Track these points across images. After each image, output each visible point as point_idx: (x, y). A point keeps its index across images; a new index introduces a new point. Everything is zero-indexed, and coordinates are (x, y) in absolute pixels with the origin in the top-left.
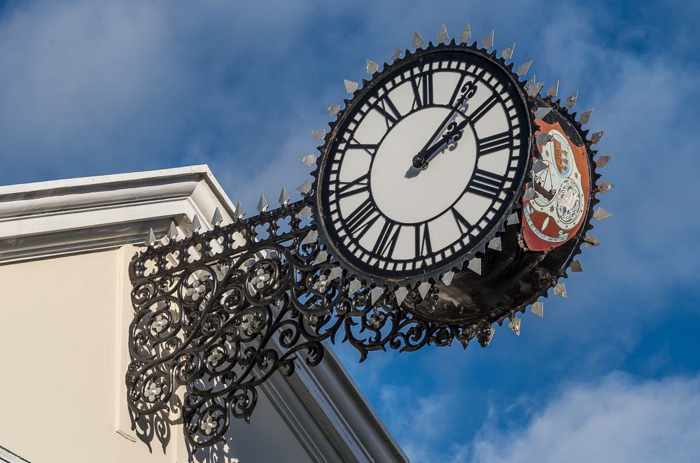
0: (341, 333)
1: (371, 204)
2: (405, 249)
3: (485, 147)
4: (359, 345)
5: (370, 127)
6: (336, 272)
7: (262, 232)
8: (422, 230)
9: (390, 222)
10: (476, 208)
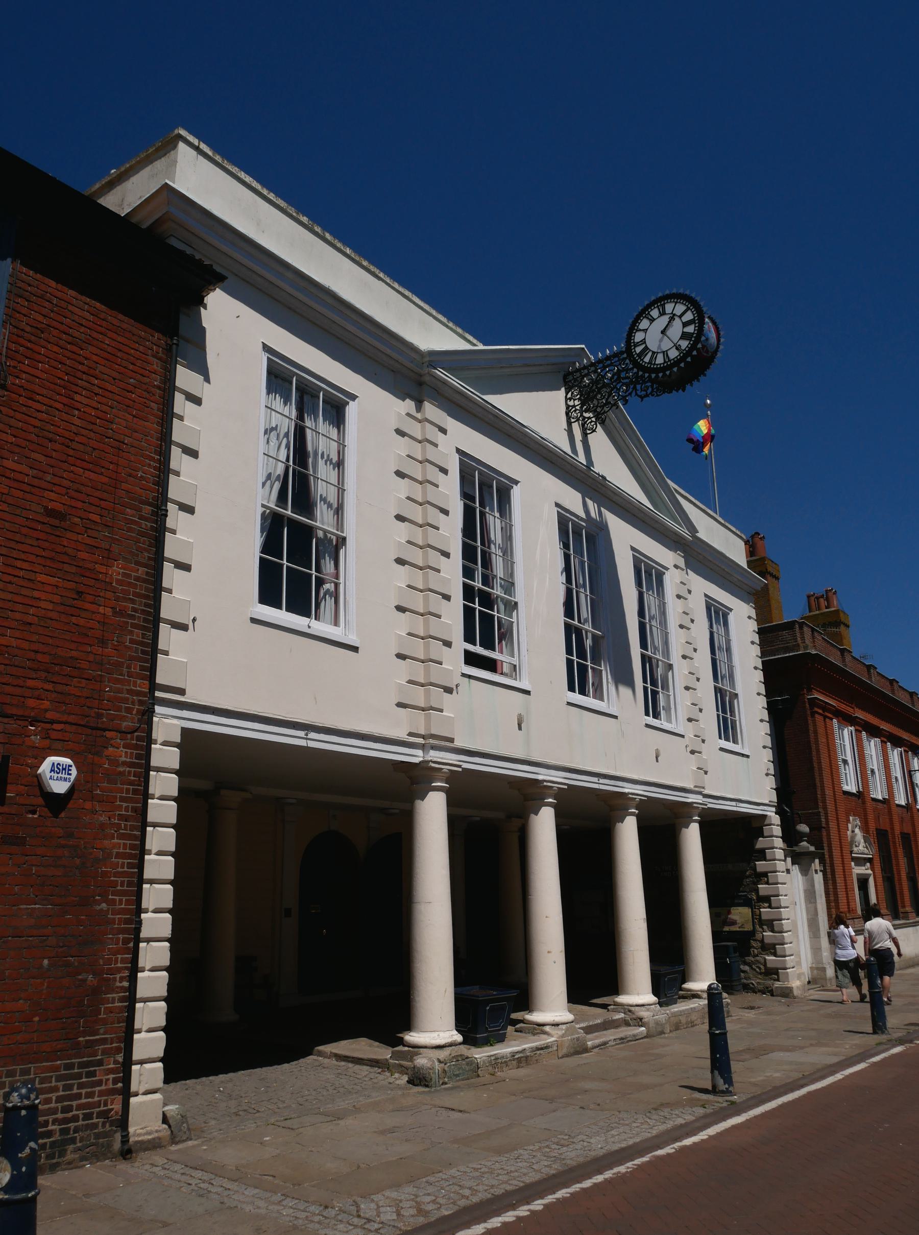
0: (634, 394)
1: (646, 348)
3: (685, 325)
5: (644, 324)
6: (635, 370)
9: (654, 353)
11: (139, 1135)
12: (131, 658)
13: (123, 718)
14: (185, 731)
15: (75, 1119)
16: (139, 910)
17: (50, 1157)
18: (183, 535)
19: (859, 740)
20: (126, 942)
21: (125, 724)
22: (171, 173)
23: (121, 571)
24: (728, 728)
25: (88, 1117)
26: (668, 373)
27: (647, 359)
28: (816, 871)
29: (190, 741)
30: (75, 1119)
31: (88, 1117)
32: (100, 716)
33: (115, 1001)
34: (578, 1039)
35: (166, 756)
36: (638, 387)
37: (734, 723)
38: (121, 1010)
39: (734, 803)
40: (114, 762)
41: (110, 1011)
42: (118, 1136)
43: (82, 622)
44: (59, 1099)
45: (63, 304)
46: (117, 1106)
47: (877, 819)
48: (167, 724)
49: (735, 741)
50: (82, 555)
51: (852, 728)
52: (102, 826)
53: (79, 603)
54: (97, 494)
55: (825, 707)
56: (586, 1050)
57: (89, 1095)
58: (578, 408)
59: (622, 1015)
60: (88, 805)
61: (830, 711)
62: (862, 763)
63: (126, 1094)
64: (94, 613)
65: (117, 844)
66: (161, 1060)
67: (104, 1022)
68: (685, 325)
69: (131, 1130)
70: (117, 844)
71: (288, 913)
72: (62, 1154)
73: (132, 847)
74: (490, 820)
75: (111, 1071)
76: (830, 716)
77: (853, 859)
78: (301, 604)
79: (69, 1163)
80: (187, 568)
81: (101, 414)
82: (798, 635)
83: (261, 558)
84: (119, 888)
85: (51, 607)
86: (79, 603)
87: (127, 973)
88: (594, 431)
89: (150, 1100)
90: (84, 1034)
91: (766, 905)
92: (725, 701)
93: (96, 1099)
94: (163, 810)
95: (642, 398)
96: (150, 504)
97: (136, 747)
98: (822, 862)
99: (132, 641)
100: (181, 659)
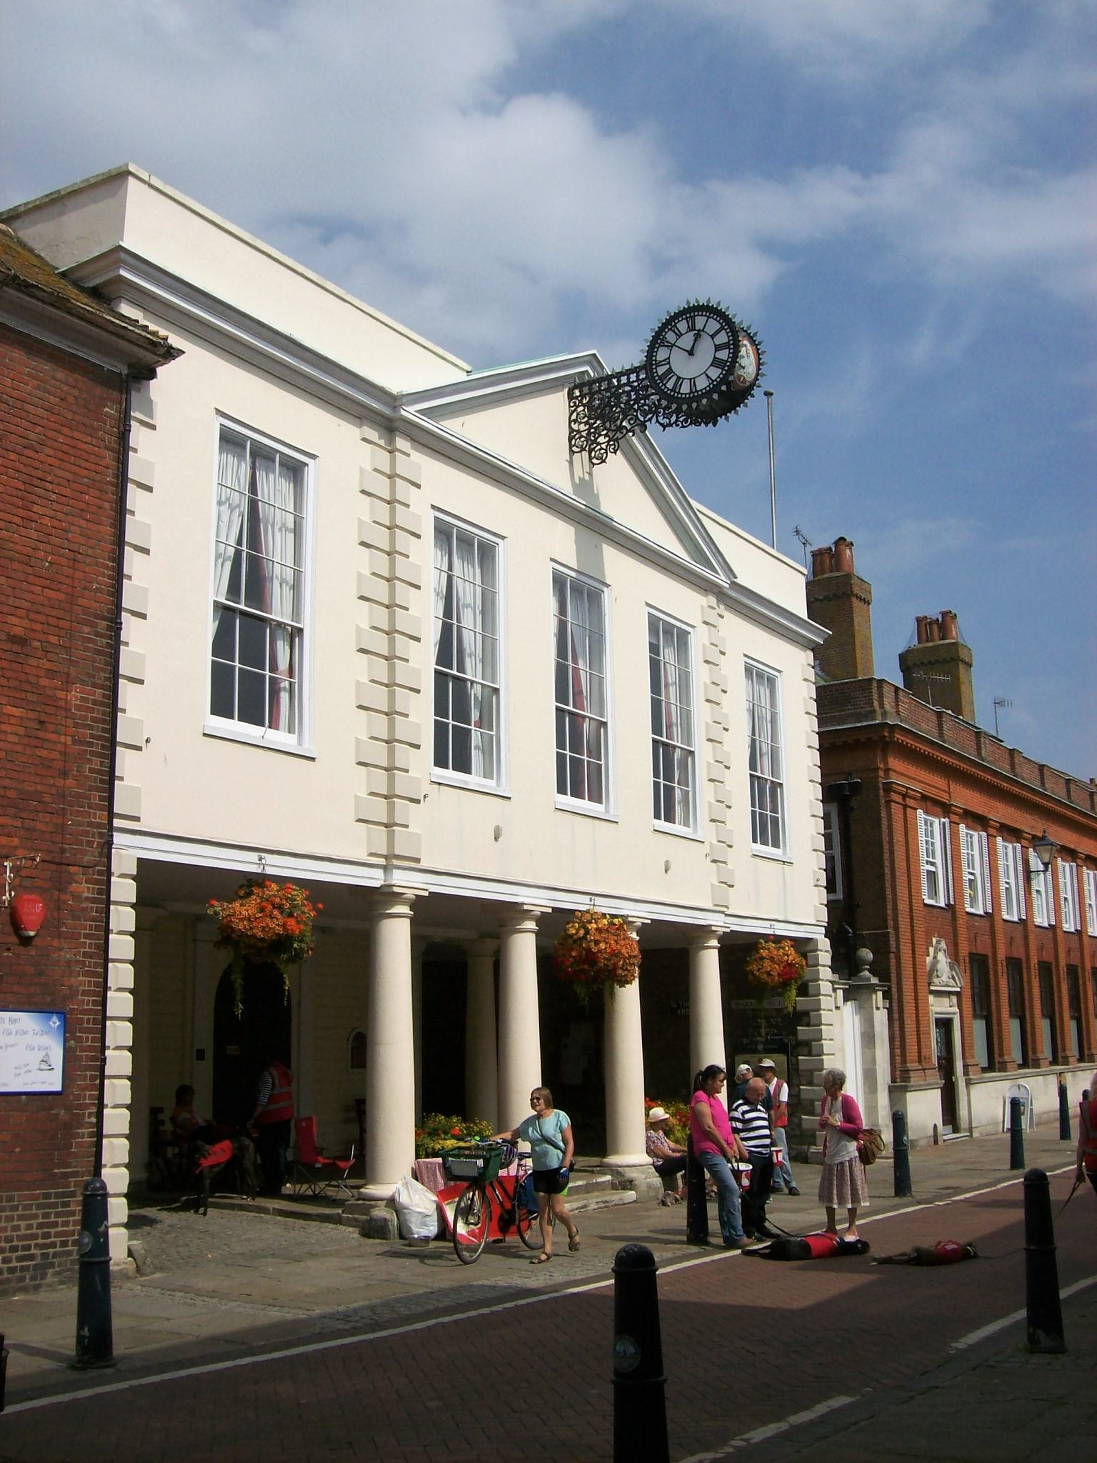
2: (685, 389)
3: (718, 348)
4: (661, 424)
7: (624, 380)
8: (692, 381)
9: (679, 378)
10: (715, 373)
12: (91, 789)
13: (85, 853)
14: (142, 862)
15: (53, 1245)
16: (103, 1048)
17: (33, 1278)
19: (955, 836)
20: (93, 1078)
21: (86, 858)
22: (121, 236)
24: (767, 828)
25: (64, 1244)
26: (694, 405)
27: (670, 385)
28: (878, 1008)
29: (148, 872)
30: (53, 1245)
31: (64, 1244)
32: (63, 851)
37: (775, 821)
38: (90, 1144)
39: (768, 924)
40: (77, 897)
41: (80, 1145)
43: (44, 753)
44: (40, 1226)
45: (19, 404)
47: (974, 939)
48: (127, 853)
49: (776, 844)
50: (44, 682)
51: (946, 820)
52: (69, 963)
53: (41, 734)
54: (55, 613)
58: (584, 434)
59: (609, 1178)
60: (56, 943)
62: (953, 862)
64: (55, 743)
66: (126, 1196)
67: (76, 1155)
68: (718, 348)
71: (200, 1055)
72: (43, 1277)
73: (96, 985)
74: (459, 948)
77: (932, 992)
78: (252, 714)
79: (50, 1286)
81: (56, 523)
82: (875, 697)
83: (213, 662)
85: (15, 739)
86: (41, 734)
87: (94, 1110)
88: (604, 461)
90: (58, 1166)
91: (806, 1052)
92: (766, 794)
93: (71, 1228)
95: (664, 427)
96: (104, 618)
97: (97, 882)
98: (887, 995)
99: (91, 771)
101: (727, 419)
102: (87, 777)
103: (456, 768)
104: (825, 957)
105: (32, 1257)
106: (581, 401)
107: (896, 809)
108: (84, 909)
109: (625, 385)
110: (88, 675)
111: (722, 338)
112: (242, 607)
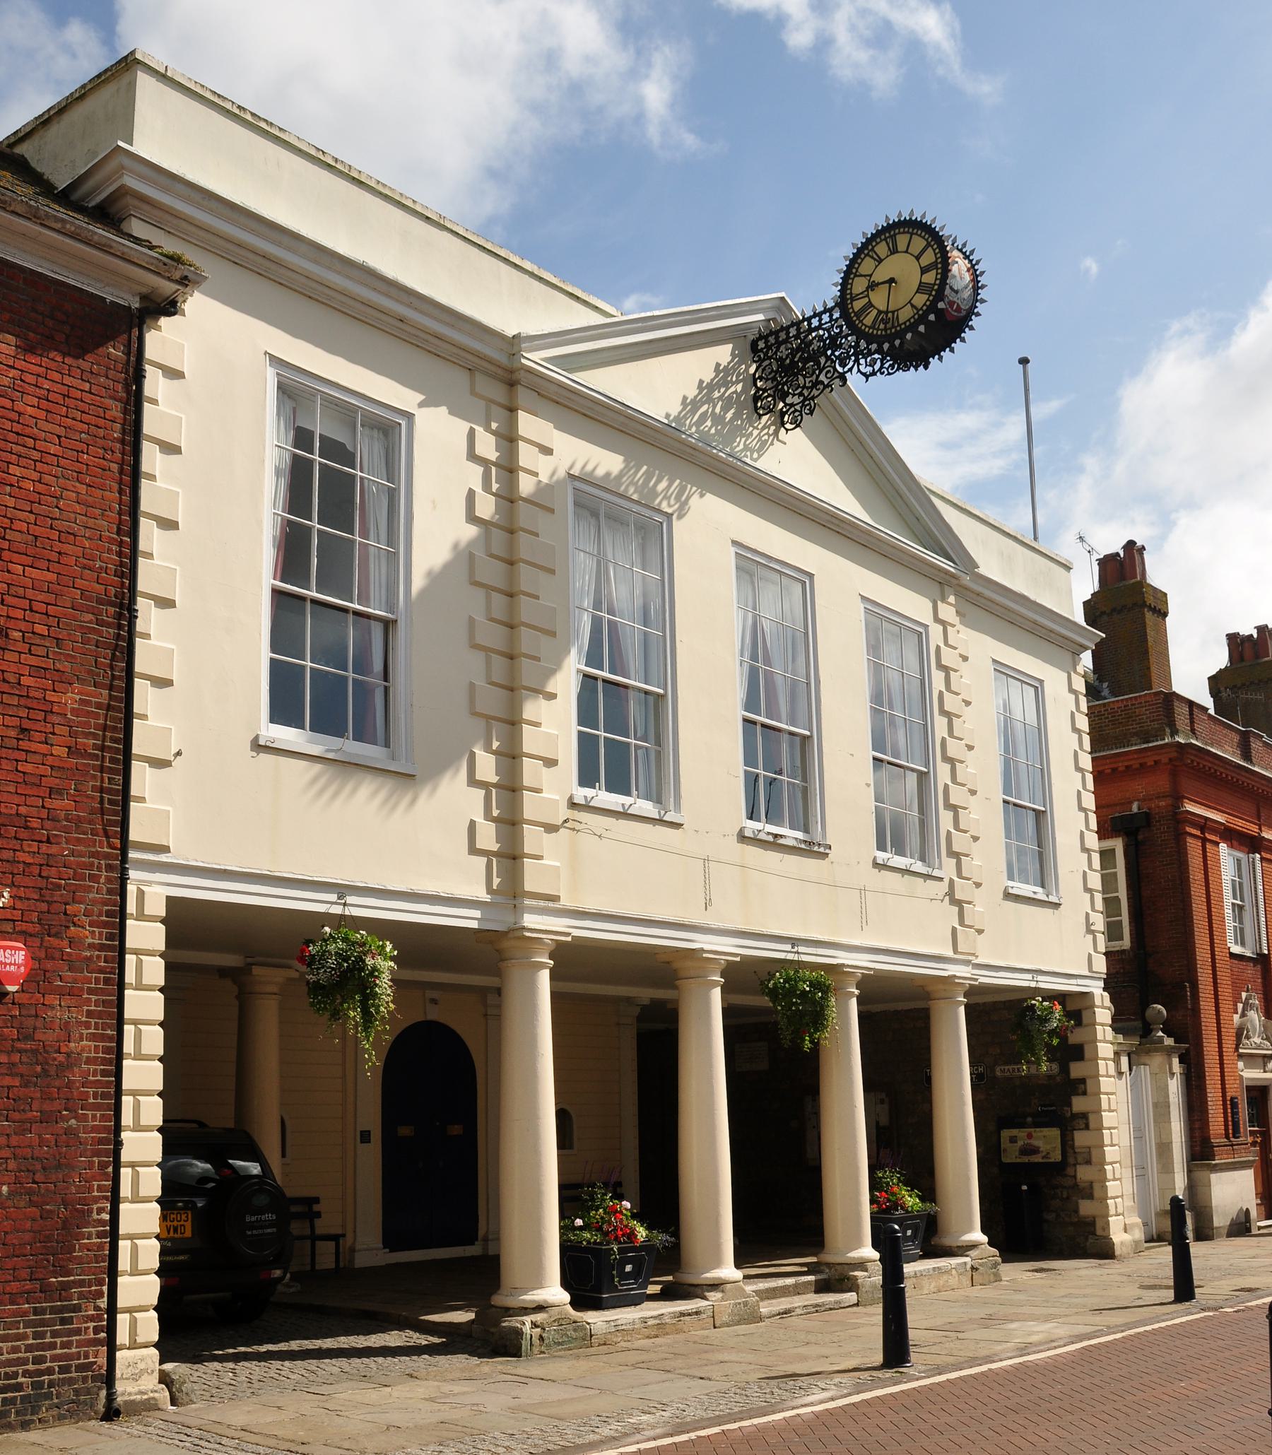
0: (855, 368)
3: (924, 271)
4: (864, 374)
11: (130, 1394)
13: (88, 889)
14: (171, 901)
15: (50, 1371)
18: (158, 639)
23: (78, 697)
26: (897, 342)
31: (63, 1370)
33: (92, 1236)
34: (746, 1304)
35: (146, 935)
36: (862, 361)
42: (103, 1393)
46: (102, 1360)
48: (150, 892)
55: (1204, 825)
56: (761, 1319)
57: (64, 1345)
61: (1214, 831)
63: (112, 1346)
65: (84, 1046)
67: (80, 1261)
69: (120, 1387)
70: (84, 1046)
71: (365, 1137)
75: (91, 1318)
76: (1217, 839)
77: (1241, 1056)
80: (167, 683)
84: (91, 1101)
89: (139, 1368)
92: (1031, 824)
94: (145, 1005)
95: (867, 376)
100: (160, 807)
101: (941, 359)
102: (87, 796)
103: (610, 789)
104: (1103, 1015)
105: (19, 1387)
106: (766, 354)
107: (1193, 846)
108: (89, 959)
109: (817, 329)
110: (89, 672)
111: (929, 258)
112: (314, 594)
